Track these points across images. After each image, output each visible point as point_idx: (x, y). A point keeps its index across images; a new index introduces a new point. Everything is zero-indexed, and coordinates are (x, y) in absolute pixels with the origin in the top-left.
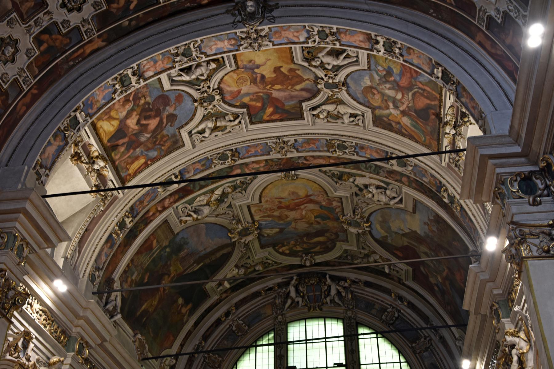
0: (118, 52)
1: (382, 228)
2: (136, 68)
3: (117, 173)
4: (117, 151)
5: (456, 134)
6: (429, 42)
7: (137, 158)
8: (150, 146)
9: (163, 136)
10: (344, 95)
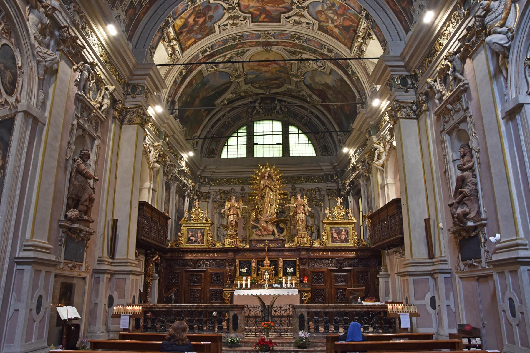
1: (310, 79)
7: (191, 39)
8: (198, 32)
9: (205, 27)
10: (305, 13)
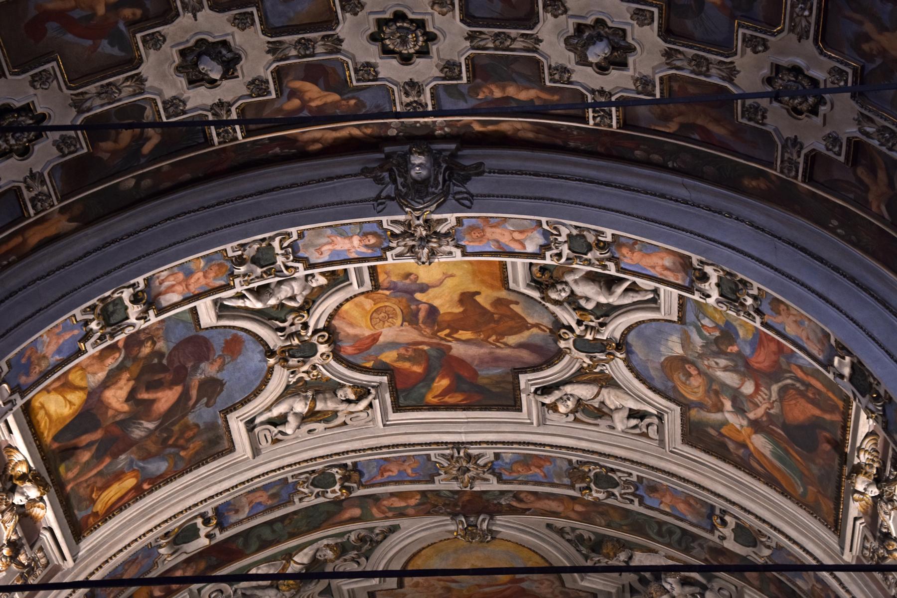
0: (104, 247)
2: (142, 286)
3: (65, 512)
4: (73, 460)
5: (880, 496)
6: (825, 294)
7: (118, 476)
8: (153, 448)
9: (187, 427)
10: (618, 368)
